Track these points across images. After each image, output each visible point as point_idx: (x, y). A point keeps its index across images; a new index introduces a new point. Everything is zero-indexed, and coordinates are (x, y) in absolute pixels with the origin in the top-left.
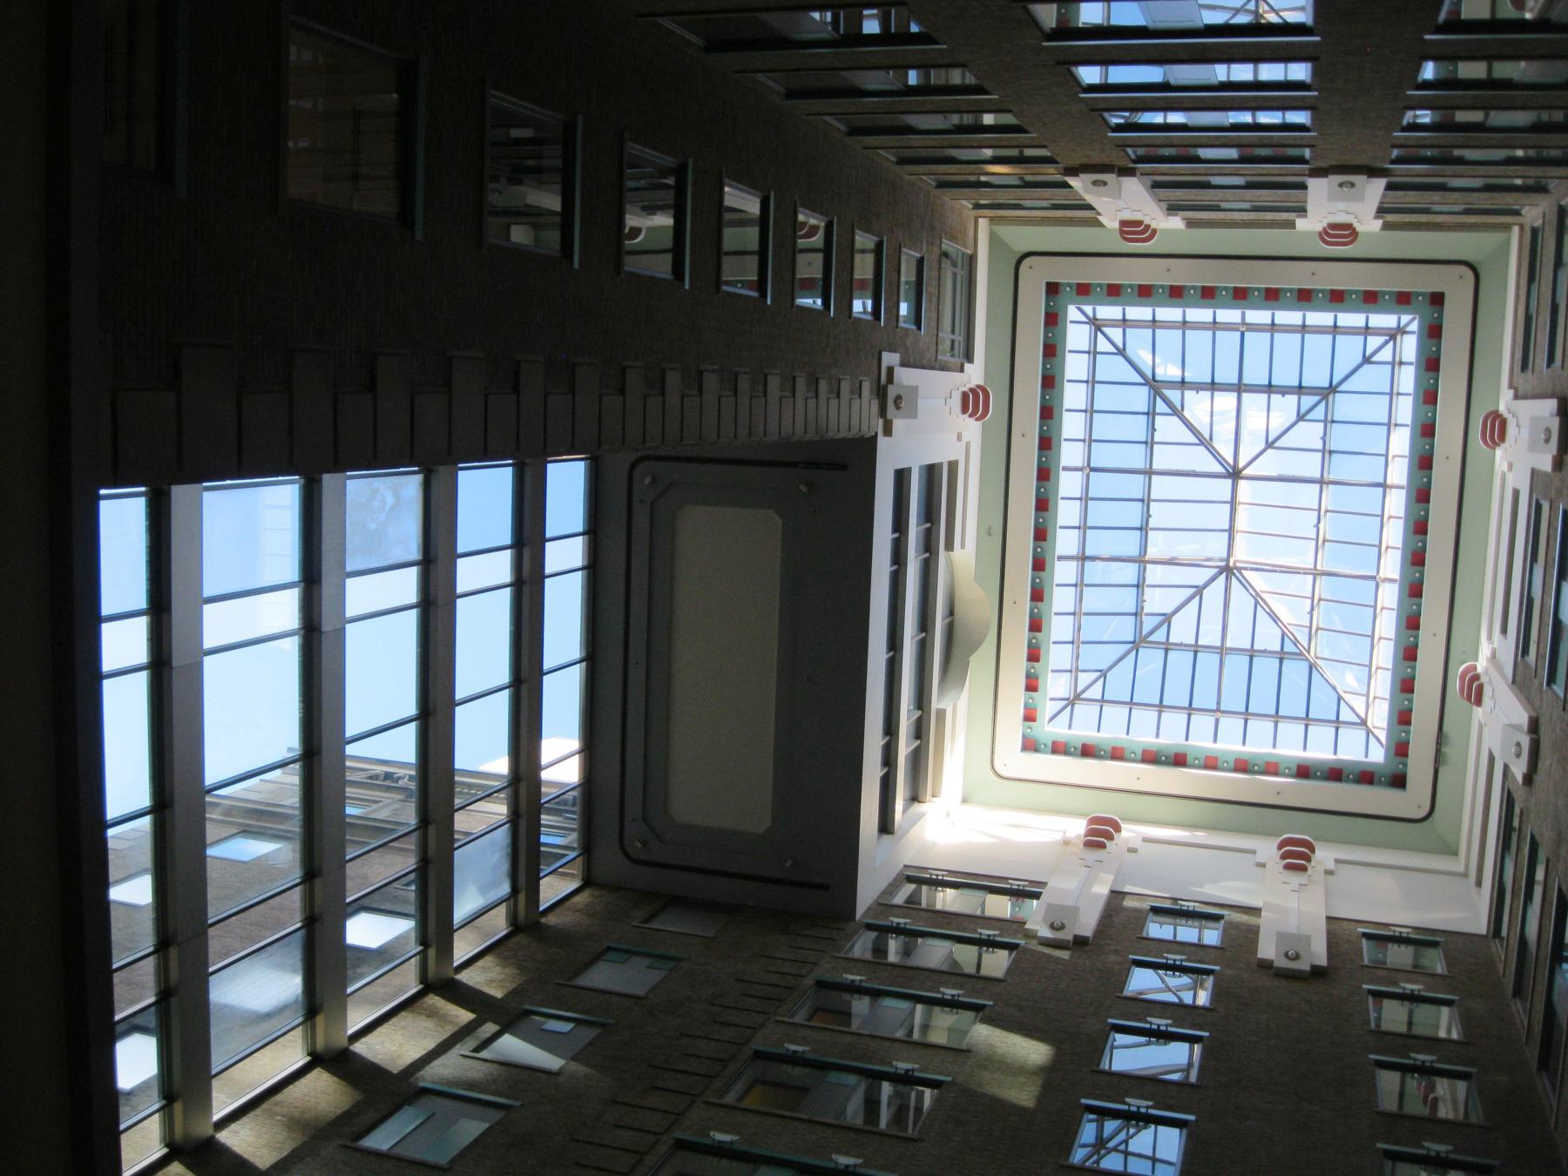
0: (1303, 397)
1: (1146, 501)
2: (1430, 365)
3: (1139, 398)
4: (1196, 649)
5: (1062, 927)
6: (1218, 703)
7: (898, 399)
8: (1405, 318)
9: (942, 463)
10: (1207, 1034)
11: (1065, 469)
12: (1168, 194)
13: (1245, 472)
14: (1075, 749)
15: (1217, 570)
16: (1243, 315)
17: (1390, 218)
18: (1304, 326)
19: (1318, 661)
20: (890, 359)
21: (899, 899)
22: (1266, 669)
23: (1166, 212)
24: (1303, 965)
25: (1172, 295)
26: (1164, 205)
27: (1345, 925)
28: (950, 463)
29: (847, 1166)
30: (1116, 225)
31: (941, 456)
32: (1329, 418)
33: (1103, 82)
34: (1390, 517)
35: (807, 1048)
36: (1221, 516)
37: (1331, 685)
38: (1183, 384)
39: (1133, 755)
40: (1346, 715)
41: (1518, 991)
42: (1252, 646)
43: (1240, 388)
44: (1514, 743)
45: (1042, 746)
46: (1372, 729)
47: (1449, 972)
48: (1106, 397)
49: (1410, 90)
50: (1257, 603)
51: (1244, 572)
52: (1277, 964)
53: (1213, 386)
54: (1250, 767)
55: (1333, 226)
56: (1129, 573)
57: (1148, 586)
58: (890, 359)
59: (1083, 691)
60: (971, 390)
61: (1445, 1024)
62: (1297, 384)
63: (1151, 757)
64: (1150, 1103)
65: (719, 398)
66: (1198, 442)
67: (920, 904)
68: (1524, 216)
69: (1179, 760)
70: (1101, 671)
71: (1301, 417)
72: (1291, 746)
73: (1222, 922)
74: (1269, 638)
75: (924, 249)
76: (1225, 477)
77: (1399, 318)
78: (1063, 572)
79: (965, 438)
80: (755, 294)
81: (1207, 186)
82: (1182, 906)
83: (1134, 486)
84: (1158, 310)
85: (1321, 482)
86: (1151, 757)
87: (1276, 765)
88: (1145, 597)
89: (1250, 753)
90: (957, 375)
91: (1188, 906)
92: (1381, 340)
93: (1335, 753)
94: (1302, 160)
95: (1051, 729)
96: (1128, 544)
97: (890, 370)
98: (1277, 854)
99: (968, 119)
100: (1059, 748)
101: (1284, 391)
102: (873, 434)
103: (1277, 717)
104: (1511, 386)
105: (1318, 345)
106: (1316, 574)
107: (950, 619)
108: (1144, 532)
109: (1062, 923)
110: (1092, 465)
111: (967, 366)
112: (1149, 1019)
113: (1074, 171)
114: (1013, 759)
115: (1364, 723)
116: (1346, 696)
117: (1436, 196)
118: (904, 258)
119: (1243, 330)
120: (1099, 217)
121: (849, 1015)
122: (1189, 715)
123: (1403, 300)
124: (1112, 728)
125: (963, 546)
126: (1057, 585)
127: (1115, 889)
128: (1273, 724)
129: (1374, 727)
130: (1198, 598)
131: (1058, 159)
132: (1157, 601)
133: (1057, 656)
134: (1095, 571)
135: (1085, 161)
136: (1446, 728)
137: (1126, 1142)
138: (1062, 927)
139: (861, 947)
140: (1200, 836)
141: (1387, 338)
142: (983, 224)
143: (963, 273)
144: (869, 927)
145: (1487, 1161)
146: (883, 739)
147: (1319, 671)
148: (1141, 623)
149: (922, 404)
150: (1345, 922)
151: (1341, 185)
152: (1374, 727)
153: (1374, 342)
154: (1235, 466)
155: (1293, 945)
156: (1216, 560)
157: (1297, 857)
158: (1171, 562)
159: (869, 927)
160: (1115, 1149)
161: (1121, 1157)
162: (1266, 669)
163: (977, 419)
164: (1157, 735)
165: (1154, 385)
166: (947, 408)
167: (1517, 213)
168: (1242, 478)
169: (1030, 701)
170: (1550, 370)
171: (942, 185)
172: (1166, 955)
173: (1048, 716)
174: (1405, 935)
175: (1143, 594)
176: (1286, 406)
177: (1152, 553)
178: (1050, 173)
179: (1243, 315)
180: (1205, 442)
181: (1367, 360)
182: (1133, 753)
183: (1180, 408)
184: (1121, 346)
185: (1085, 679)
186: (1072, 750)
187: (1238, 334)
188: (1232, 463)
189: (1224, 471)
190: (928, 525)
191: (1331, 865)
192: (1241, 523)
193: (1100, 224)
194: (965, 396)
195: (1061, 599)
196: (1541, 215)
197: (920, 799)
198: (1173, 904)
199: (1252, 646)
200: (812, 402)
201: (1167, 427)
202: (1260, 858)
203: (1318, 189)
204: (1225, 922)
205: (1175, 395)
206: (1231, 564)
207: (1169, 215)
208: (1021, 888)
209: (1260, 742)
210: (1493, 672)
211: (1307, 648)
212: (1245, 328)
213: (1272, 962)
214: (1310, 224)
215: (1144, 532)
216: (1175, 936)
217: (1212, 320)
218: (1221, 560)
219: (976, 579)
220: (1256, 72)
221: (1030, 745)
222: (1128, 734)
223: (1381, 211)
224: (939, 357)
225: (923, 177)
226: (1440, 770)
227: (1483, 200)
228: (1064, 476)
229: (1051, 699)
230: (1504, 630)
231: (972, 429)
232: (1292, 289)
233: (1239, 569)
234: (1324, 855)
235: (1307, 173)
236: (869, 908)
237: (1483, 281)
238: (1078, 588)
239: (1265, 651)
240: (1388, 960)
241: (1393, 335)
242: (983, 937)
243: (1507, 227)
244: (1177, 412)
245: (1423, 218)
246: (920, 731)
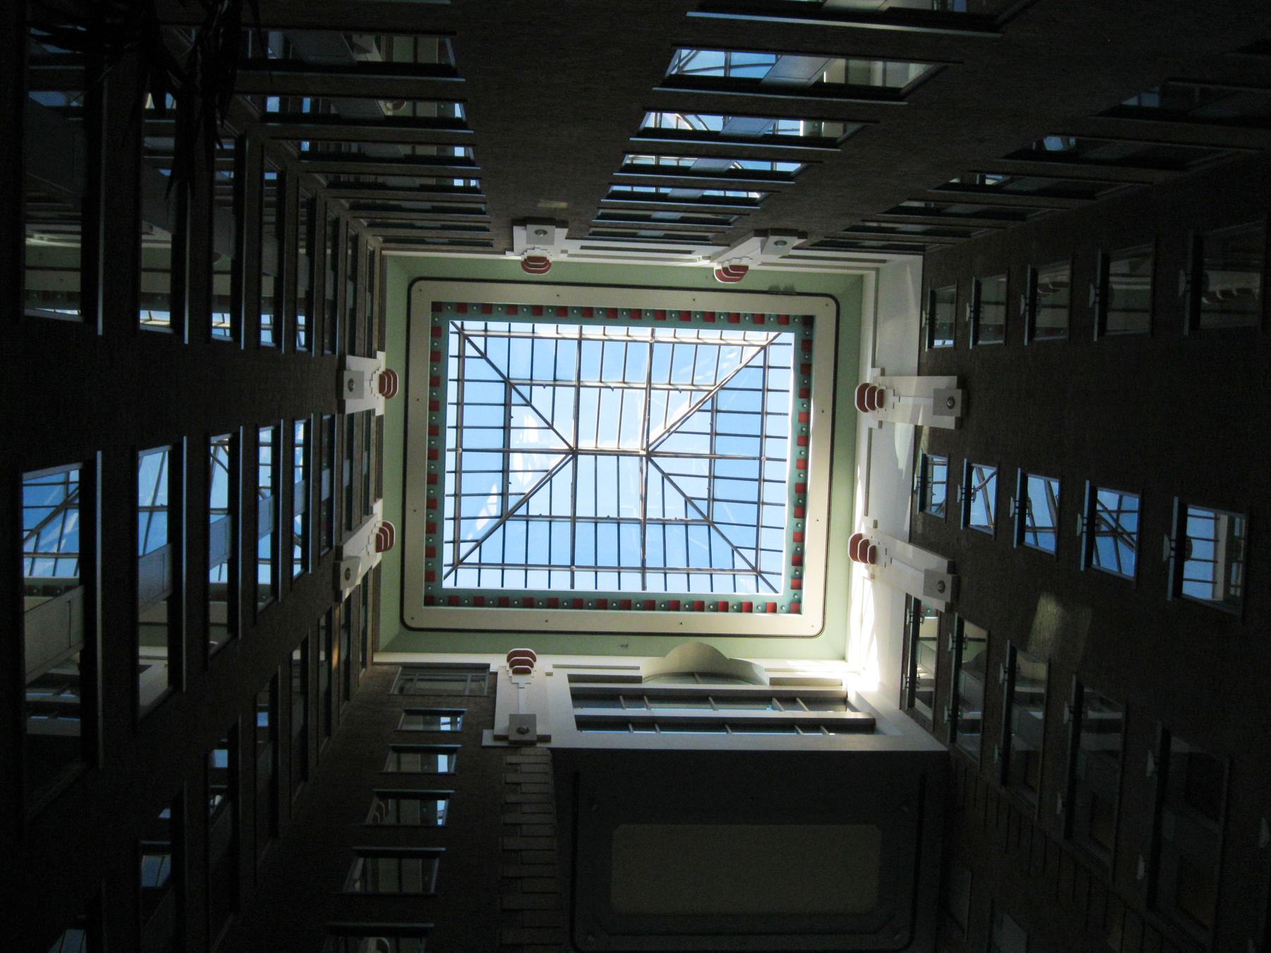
0: (513, 402)
1: (596, 521)
2: (486, 311)
3: (515, 528)
4: (712, 477)
5: (942, 583)
6: (754, 459)
7: (521, 731)
8: (452, 328)
9: (572, 689)
10: (1019, 470)
11: (572, 586)
12: (356, 517)
13: (572, 444)
14: (796, 571)
15: (649, 463)
16: (450, 450)
17: (375, 346)
18: (459, 357)
19: (718, 383)
20: (487, 739)
21: (928, 713)
22: (724, 424)
23: (370, 515)
24: (958, 395)
25: (437, 434)
26: (365, 517)
27: (924, 361)
28: (570, 681)
29: (1156, 764)
30: (379, 555)
31: (565, 687)
32: (529, 382)
33: (269, 562)
34: (604, 335)
35: (1059, 795)
36: (607, 463)
37: (736, 374)
38: (504, 494)
39: (799, 525)
41: (966, 234)
42: (708, 434)
43: (506, 451)
44: (776, 246)
45: (796, 597)
46: (769, 340)
47: (954, 283)
48: (515, 556)
49: (281, 351)
50: (675, 432)
51: (650, 443)
52: (959, 415)
53: (505, 471)
54: (803, 434)
55: (381, 390)
56: (654, 532)
57: (664, 516)
58: (487, 739)
59: (750, 565)
60: (511, 666)
61: (994, 287)
62: (503, 407)
63: (800, 511)
64: (1079, 516)
65: (524, 893)
66: (549, 483)
67: (931, 693)
68: (375, 248)
69: (801, 490)
70: (733, 551)
71: (528, 403)
72: (785, 402)
73: (929, 456)
74: (701, 421)
75: (399, 709)
76: (577, 460)
77: (452, 333)
78: (655, 585)
79: (550, 669)
80: (437, 863)
81: (350, 488)
82: (917, 487)
83: (585, 530)
84: (447, 469)
85: (578, 387)
86: (800, 511)
87: (800, 414)
88: (673, 518)
89: (787, 547)
90: (500, 677)
91: (918, 482)
92: (468, 345)
93: (789, 368)
94: (332, 421)
95: (783, 594)
96: (631, 534)
97: (497, 738)
98: (870, 414)
99: (296, 672)
100: (797, 584)
101: (508, 416)
102: (549, 751)
103: (762, 437)
104: (504, 253)
105: (472, 392)
106: (649, 387)
107: (697, 676)
108: (621, 521)
109: (949, 399)
110: (569, 564)
111: (492, 669)
112: (1011, 515)
113: (338, 594)
114: (808, 620)
115: (764, 348)
116: (744, 362)
117: (359, 315)
118: (405, 727)
119: (461, 449)
120: (373, 568)
121: (1027, 753)
122: (765, 481)
123: (439, 333)
124: (778, 540)
125: (638, 668)
126: (666, 590)
127: (916, 370)
128: (768, 416)
129: (767, 339)
131: (328, 608)
132: (676, 509)
133: (723, 588)
134: (654, 560)
135: (330, 586)
136: (765, 288)
137: (1109, 512)
138: (942, 583)
139: (969, 743)
140: (861, 472)
141: (466, 341)
142: (378, 658)
143: (417, 674)
144: (953, 739)
145: (1099, 257)
146: (798, 732)
147: (726, 382)
148: (693, 520)
149: (523, 710)
150: (921, 361)
151: (351, 389)
152: (767, 339)
153: (470, 350)
154: (567, 453)
155: (941, 403)
156: (642, 464)
157: (873, 398)
158: (644, 499)
159: (953, 739)
160: (1116, 521)
161: (1122, 516)
162: (724, 424)
163: (535, 660)
164: (784, 505)
165: (505, 516)
166: (526, 686)
167: (373, 253)
168: (577, 447)
169: (760, 608)
170: (491, 230)
171: (347, 696)
172: (958, 501)
173: (773, 594)
174: (928, 315)
175: (670, 520)
176: (521, 415)
177: (637, 514)
178: (339, 612)
179: (450, 450)
180: (550, 475)
181: (484, 356)
182: (800, 453)
183: (523, 496)
184: (474, 544)
185: (740, 564)
186: (797, 573)
187: (464, 454)
188: (564, 456)
189: (571, 461)
190: (621, 698)
191: (878, 371)
192: (611, 445)
193: (379, 565)
194: (516, 672)
195: (677, 586)
196: (375, 237)
197: (845, 695)
198: (917, 493)
199: (708, 434)
200: (525, 808)
201: (538, 505)
202: (875, 426)
203: (353, 406)
204: (929, 453)
205: (512, 501)
206: (644, 453)
207: (372, 513)
208: (912, 614)
209: (783, 425)
210: (721, 259)
211: (707, 393)
212: (459, 448)
213: (957, 418)
214: (379, 405)
215: (621, 521)
216: (943, 483)
217: (454, 474)
218: (641, 460)
219: (664, 656)
220: (265, 445)
221: (796, 608)
222: (783, 528)
223: (371, 354)
224: (485, 694)
225: (341, 712)
226: (798, 290)
227: (363, 281)
228: (578, 588)
229: (758, 591)
230: (689, 252)
231: (543, 663)
232: (429, 440)
233: (648, 446)
234: (869, 375)
235: (341, 415)
236: (938, 739)
237: (425, 274)
238: (667, 571)
239: (712, 425)
240: (948, 322)
241: (464, 337)
242: (955, 646)
243: (383, 258)
244: (526, 499)
245: (376, 321)
246: (789, 699)
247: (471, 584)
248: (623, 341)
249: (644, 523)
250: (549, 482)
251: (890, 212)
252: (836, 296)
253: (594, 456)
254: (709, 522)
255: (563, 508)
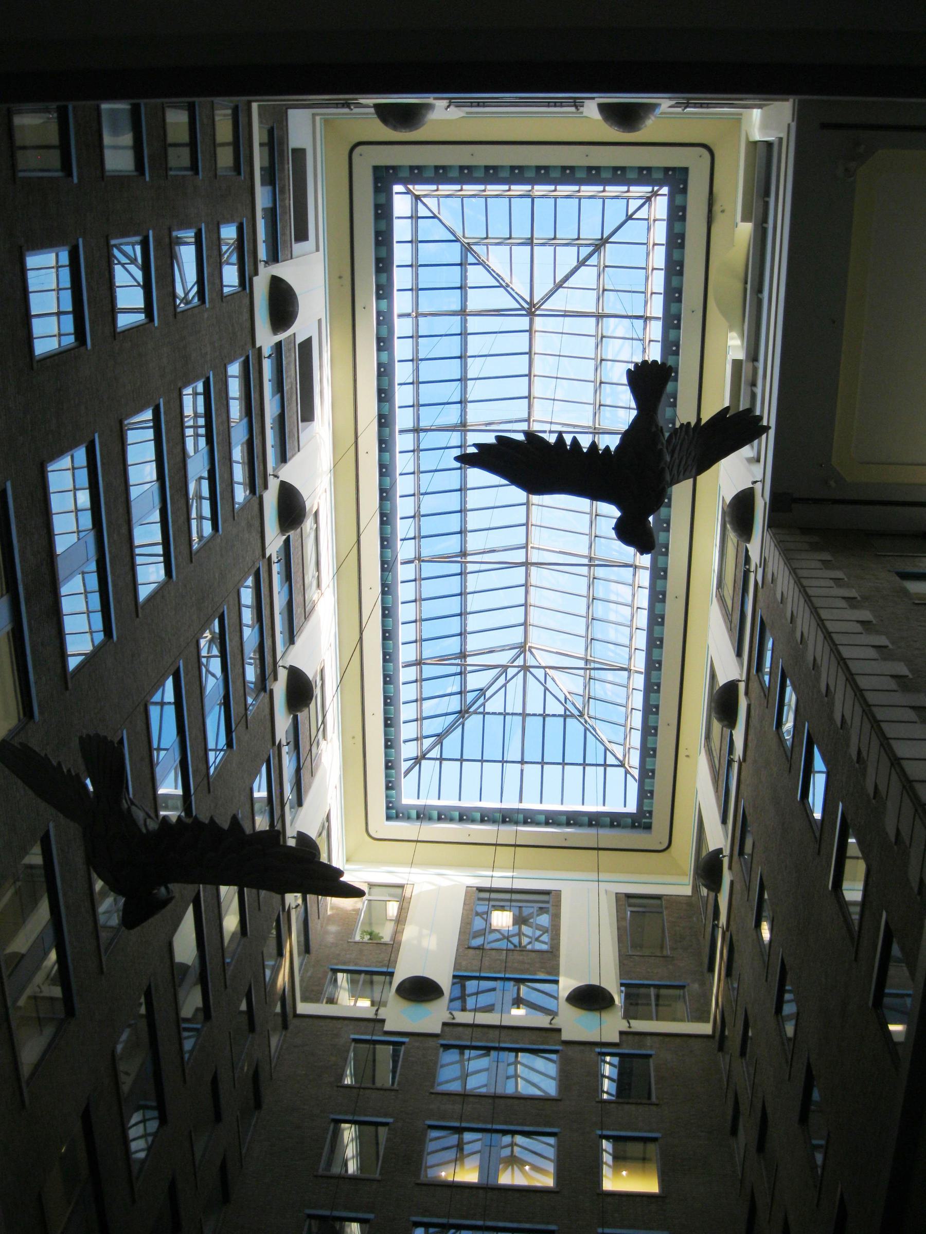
40: (611, 760)
56: (454, 324)
74: (555, 707)
116: (609, 746)
129: (630, 767)
130: (505, 674)
134: (427, 440)
137: (484, 705)
160: (475, 712)
181: (629, 218)
221: (394, 812)
228: (401, 587)
247: (400, 490)
248: (646, 288)
249: (463, 655)
250: (498, 284)
251: (762, 622)
252: (669, 850)
253: (528, 328)
254: (463, 713)
255: (476, 301)
